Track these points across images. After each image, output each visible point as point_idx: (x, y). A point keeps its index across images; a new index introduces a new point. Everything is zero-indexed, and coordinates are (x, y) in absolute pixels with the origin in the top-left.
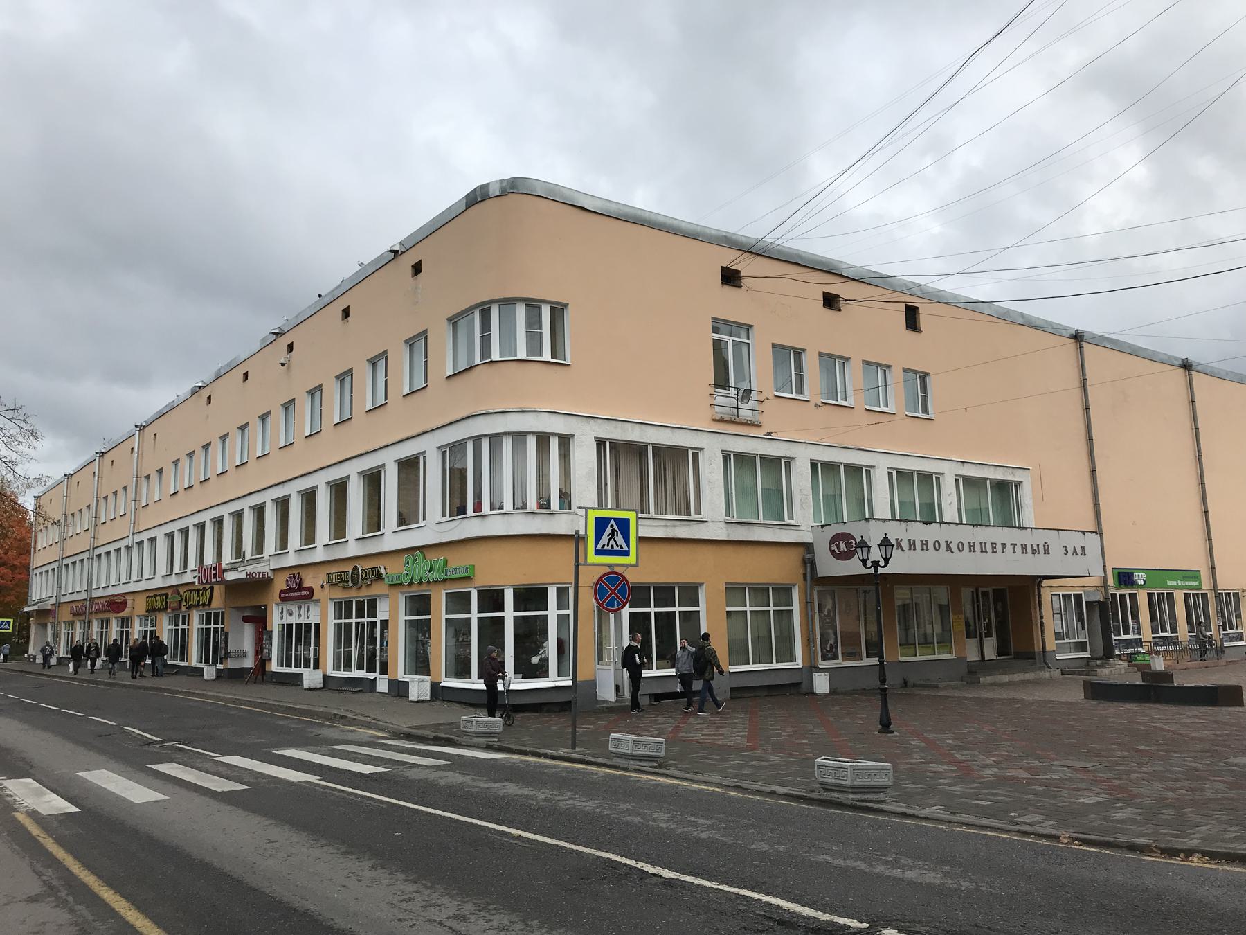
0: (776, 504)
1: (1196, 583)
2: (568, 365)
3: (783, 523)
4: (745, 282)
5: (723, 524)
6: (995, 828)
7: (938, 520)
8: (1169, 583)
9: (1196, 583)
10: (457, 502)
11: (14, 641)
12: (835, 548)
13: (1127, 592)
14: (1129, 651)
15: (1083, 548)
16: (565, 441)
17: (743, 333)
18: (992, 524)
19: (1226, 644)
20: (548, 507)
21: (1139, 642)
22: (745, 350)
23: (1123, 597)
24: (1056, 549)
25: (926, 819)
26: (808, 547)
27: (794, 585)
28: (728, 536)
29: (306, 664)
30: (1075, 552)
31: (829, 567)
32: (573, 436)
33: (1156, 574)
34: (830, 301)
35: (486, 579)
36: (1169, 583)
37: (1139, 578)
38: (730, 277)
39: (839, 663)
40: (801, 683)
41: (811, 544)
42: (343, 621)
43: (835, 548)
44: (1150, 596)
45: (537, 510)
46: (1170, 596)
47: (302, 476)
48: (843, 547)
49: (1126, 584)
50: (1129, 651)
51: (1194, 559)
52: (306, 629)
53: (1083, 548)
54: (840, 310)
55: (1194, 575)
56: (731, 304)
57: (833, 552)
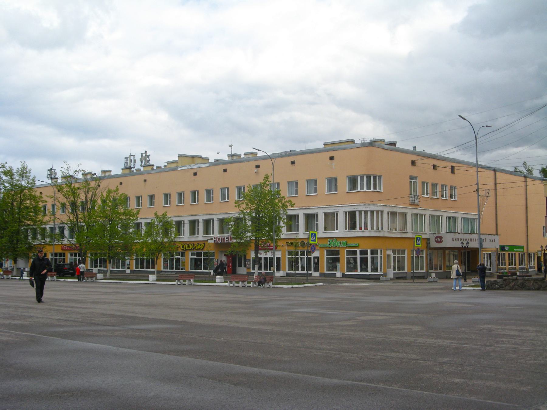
0: (403, 228)
1: (522, 250)
2: (382, 192)
3: (423, 232)
4: (417, 164)
5: (411, 233)
6: (95, 324)
7: (452, 232)
8: (515, 250)
9: (522, 250)
10: (378, 228)
11: (330, 261)
12: (436, 240)
13: (503, 253)
14: (502, 271)
15: (494, 240)
16: (382, 212)
17: (415, 179)
18: (452, 232)
19: (530, 270)
20: (379, 230)
21: (505, 269)
22: (415, 183)
23: (502, 254)
24: (488, 240)
25: (383, 316)
26: (428, 239)
27: (406, 249)
28: (412, 236)
29: (363, 267)
30: (492, 241)
31: (434, 244)
32: (383, 211)
33: (512, 247)
34: (434, 167)
35: (363, 247)
36: (515, 250)
37: (507, 248)
38: (271, 175)
39: (439, 271)
40: (424, 276)
41: (429, 238)
42: (396, 256)
43: (436, 240)
44: (509, 254)
45: (377, 230)
46: (515, 254)
47: (496, 214)
48: (439, 240)
49: (503, 250)
50: (502, 271)
51: (523, 243)
52: (173, 266)
53: (494, 240)
54: (436, 169)
55: (522, 247)
56: (413, 171)
57: (436, 241)
